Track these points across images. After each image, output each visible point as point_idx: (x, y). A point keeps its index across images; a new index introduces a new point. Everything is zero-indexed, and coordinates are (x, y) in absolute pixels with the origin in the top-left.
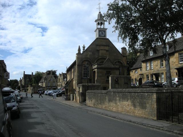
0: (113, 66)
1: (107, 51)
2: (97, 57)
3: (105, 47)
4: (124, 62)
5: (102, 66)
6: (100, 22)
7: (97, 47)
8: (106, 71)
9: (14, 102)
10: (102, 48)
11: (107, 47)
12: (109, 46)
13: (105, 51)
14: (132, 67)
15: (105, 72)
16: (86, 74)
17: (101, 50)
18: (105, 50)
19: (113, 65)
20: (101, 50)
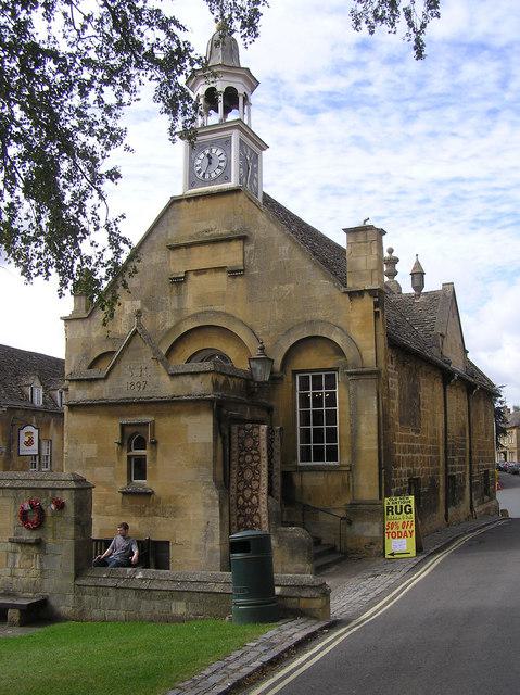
0: (167, 387)
1: (234, 273)
2: (169, 325)
3: (222, 248)
4: (357, 335)
5: (98, 387)
6: (220, 87)
7: (173, 255)
8: (123, 426)
9: (258, 514)
10: (202, 258)
11: (236, 246)
12: (244, 239)
13: (223, 276)
14: (27, 396)
15: (111, 428)
16: (318, 415)
17: (198, 272)
18: (222, 269)
19: (172, 375)
20: (198, 272)
